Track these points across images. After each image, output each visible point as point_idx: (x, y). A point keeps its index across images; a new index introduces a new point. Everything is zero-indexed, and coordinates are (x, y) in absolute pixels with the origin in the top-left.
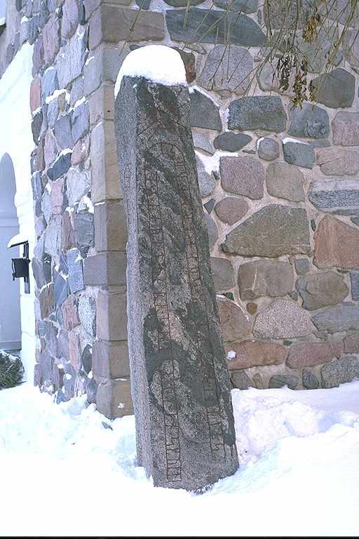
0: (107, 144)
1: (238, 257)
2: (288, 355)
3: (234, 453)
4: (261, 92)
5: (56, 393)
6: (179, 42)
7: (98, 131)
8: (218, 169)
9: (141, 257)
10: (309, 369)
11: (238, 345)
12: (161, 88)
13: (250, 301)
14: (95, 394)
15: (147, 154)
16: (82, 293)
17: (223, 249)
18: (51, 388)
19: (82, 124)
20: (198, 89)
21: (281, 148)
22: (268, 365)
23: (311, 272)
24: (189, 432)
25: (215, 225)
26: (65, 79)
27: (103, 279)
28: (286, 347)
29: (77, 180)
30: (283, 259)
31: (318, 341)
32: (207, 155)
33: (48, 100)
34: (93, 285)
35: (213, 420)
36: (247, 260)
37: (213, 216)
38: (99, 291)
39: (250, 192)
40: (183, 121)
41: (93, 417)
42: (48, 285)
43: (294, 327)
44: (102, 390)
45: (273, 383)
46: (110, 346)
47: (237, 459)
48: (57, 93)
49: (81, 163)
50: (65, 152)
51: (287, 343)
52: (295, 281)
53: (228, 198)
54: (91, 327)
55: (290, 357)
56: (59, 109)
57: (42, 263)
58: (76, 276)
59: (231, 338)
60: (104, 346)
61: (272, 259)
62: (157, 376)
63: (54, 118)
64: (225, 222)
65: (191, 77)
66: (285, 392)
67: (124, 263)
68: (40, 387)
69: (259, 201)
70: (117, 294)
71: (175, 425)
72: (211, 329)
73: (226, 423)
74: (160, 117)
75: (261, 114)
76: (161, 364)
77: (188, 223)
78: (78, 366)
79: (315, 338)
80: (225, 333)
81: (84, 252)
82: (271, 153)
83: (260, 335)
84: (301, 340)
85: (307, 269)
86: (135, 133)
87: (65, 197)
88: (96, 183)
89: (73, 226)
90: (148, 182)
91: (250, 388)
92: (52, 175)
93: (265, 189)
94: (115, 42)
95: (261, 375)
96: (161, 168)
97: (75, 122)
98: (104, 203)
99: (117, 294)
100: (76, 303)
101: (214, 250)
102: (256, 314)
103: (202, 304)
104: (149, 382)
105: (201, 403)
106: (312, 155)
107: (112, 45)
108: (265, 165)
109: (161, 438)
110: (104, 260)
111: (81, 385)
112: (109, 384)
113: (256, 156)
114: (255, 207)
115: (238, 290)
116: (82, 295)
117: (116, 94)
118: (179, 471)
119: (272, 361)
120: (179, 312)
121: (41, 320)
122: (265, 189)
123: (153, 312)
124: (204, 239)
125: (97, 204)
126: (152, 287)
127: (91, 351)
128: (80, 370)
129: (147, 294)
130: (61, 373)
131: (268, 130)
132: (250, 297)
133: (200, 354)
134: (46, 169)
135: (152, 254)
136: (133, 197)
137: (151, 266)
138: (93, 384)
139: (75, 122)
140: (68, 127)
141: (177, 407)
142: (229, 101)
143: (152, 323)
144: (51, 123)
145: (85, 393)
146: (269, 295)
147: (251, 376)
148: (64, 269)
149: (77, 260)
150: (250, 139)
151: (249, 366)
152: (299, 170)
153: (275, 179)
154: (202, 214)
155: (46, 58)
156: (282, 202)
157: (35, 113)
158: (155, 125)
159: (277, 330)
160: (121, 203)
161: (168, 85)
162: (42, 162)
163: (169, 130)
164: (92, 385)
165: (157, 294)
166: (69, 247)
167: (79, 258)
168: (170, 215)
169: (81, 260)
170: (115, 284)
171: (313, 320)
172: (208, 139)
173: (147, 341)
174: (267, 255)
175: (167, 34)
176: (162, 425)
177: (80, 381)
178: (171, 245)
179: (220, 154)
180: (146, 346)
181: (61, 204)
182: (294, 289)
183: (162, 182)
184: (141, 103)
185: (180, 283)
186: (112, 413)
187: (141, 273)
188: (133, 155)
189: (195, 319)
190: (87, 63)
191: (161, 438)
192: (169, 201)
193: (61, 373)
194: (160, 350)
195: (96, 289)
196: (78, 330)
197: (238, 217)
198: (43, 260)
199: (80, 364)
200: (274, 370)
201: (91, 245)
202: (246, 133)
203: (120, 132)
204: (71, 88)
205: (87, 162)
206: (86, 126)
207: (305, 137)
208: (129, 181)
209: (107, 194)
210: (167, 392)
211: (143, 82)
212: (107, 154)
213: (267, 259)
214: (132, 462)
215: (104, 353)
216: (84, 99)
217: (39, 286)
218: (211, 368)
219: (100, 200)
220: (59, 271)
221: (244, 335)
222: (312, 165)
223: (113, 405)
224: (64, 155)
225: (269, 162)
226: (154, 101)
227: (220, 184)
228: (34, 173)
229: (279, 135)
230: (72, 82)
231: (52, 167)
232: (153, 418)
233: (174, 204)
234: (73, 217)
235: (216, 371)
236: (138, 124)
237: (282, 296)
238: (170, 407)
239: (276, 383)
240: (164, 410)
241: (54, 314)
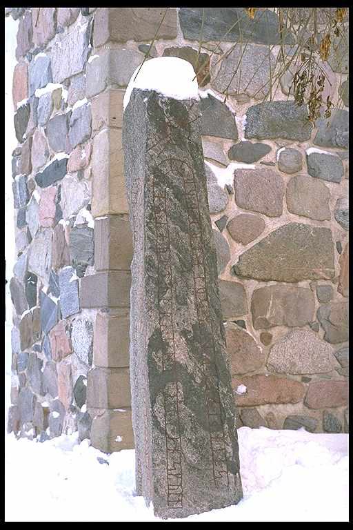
0: (111, 154)
1: (252, 281)
2: (307, 394)
3: (238, 482)
4: (283, 96)
5: (39, 436)
6: (192, 41)
7: (101, 137)
8: (231, 183)
9: (147, 275)
10: (330, 411)
11: (251, 379)
12: (172, 101)
13: (265, 331)
14: (89, 429)
15: (156, 171)
16: (77, 317)
17: (236, 271)
18: (32, 432)
19: (83, 128)
20: (213, 93)
21: (304, 160)
22: (284, 403)
23: (336, 301)
24: (191, 457)
25: (227, 245)
26: (62, 72)
27: (103, 299)
28: (304, 384)
29: (74, 192)
30: (303, 284)
31: (341, 379)
32: (221, 167)
33: (39, 93)
34: (90, 308)
35: (216, 446)
36: (262, 285)
37: (225, 234)
38: (98, 314)
39: (267, 208)
40: (194, 136)
41: (88, 453)
42: (32, 309)
43: (313, 362)
44: (98, 423)
45: (289, 424)
46: (109, 374)
47: (241, 489)
48: (51, 87)
49: (81, 172)
50: (60, 156)
51: (305, 380)
52: (316, 310)
53: (241, 215)
54: (86, 354)
55: (308, 396)
56: (53, 105)
57: (24, 285)
58: (70, 298)
59: (241, 370)
60: (102, 374)
61: (291, 284)
62: (160, 398)
63: (46, 115)
64: (238, 241)
65: (203, 80)
66: (302, 434)
67: (129, 282)
68: (15, 434)
69: (277, 219)
70: (118, 317)
71: (178, 449)
72: (218, 352)
73: (230, 450)
74: (169, 132)
75: (282, 121)
76: (165, 385)
77: (196, 243)
78: (68, 401)
79: (338, 375)
80: (235, 367)
81: (81, 273)
82: (294, 165)
83: (275, 370)
84: (322, 377)
85: (331, 297)
86: (144, 149)
87: (58, 207)
88: (98, 195)
89: (67, 241)
90: (156, 199)
91: (262, 427)
92: (42, 181)
93: (285, 205)
94: (123, 42)
95: (275, 414)
96: (170, 185)
97: (74, 124)
98: (106, 217)
99: (118, 317)
100: (69, 329)
101: (226, 272)
102: (270, 346)
103: (209, 326)
104: (152, 404)
105: (205, 429)
106: (339, 168)
107: (119, 46)
108: (286, 178)
109: (163, 462)
110: (104, 280)
111: (72, 422)
112: (107, 414)
113: (275, 169)
114: (272, 225)
115: (251, 317)
116: (76, 319)
117: (125, 105)
118: (180, 498)
119: (288, 399)
120: (184, 333)
121: (20, 352)
122: (285, 205)
123: (158, 332)
124: (212, 259)
125: (99, 219)
126: (158, 306)
127: (85, 382)
128: (71, 405)
129: (153, 314)
130: (46, 412)
131: (289, 139)
132: (263, 326)
133: (204, 380)
134: (34, 173)
135: (158, 272)
136: (140, 213)
137: (157, 285)
138: (87, 419)
139: (74, 124)
140: (64, 128)
141: (181, 431)
142: (246, 107)
143: (157, 343)
144: (42, 120)
145: (77, 430)
146: (286, 325)
147: (263, 415)
148: (54, 290)
149: (71, 281)
150: (269, 149)
151: (260, 402)
152: (324, 185)
153: (296, 194)
154: (211, 232)
155: (35, 40)
156: (304, 221)
157: (19, 105)
158: (165, 141)
159: (294, 364)
160: (125, 218)
161: (179, 99)
162: (28, 164)
163: (180, 146)
164: (86, 420)
165: (162, 314)
166: (62, 266)
167: (75, 277)
168: (177, 233)
169: (77, 281)
170: (117, 306)
171: (336, 355)
172: (222, 148)
173: (151, 362)
174: (285, 280)
175: (180, 32)
176: (164, 449)
177: (71, 418)
178: (179, 264)
179: (235, 165)
180: (149, 367)
181: (53, 215)
182: (315, 318)
183: (171, 200)
184: (151, 118)
185: (186, 304)
186: (109, 448)
187: (147, 292)
188: (141, 170)
189: (200, 340)
190: (90, 61)
191: (163, 462)
192: (177, 219)
193: (46, 412)
194: (163, 371)
195: (94, 313)
196: (69, 360)
197: (254, 237)
198: (26, 281)
199: (71, 398)
200: (290, 410)
201: (89, 263)
202: (266, 142)
203: (128, 144)
204: (69, 84)
205: (87, 172)
206: (88, 130)
207: (334, 147)
208: (136, 198)
209: (110, 208)
210: (171, 415)
211: (154, 95)
212: (111, 165)
213: (285, 284)
214: (131, 493)
215: (102, 379)
216: (85, 100)
217: (19, 311)
218: (216, 393)
219: (103, 214)
220: (48, 293)
221: (256, 368)
222: (339, 179)
223: (110, 438)
224: (59, 160)
225: (289, 175)
226: (169, 122)
227: (233, 199)
228: (17, 177)
229: (302, 145)
230: (71, 77)
231: (42, 172)
232: (155, 441)
233: (182, 222)
234: (69, 231)
235: (221, 396)
236: (148, 139)
237: (301, 326)
238: (172, 431)
239: (292, 423)
240: (166, 433)
241: (39, 343)
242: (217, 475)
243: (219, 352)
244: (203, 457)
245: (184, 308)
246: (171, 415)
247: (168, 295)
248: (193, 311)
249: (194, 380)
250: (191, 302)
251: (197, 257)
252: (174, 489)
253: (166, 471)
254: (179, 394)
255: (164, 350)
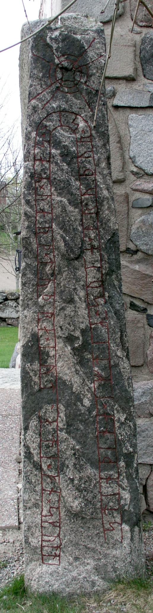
62: (34, 423)
120: (70, 339)
133: (95, 399)
163: (74, 93)
176: (39, 488)
192: (64, 188)
218: (108, 419)
235: (117, 425)
238: (49, 466)
240: (41, 469)
242: (107, 526)
243: (117, 365)
244: (88, 502)
245: (69, 310)
246: (48, 447)
247: (49, 288)
248: (83, 311)
249: (81, 401)
250: (80, 299)
251: (90, 239)
252: (50, 541)
253: (39, 516)
254: (59, 419)
255: (43, 362)
